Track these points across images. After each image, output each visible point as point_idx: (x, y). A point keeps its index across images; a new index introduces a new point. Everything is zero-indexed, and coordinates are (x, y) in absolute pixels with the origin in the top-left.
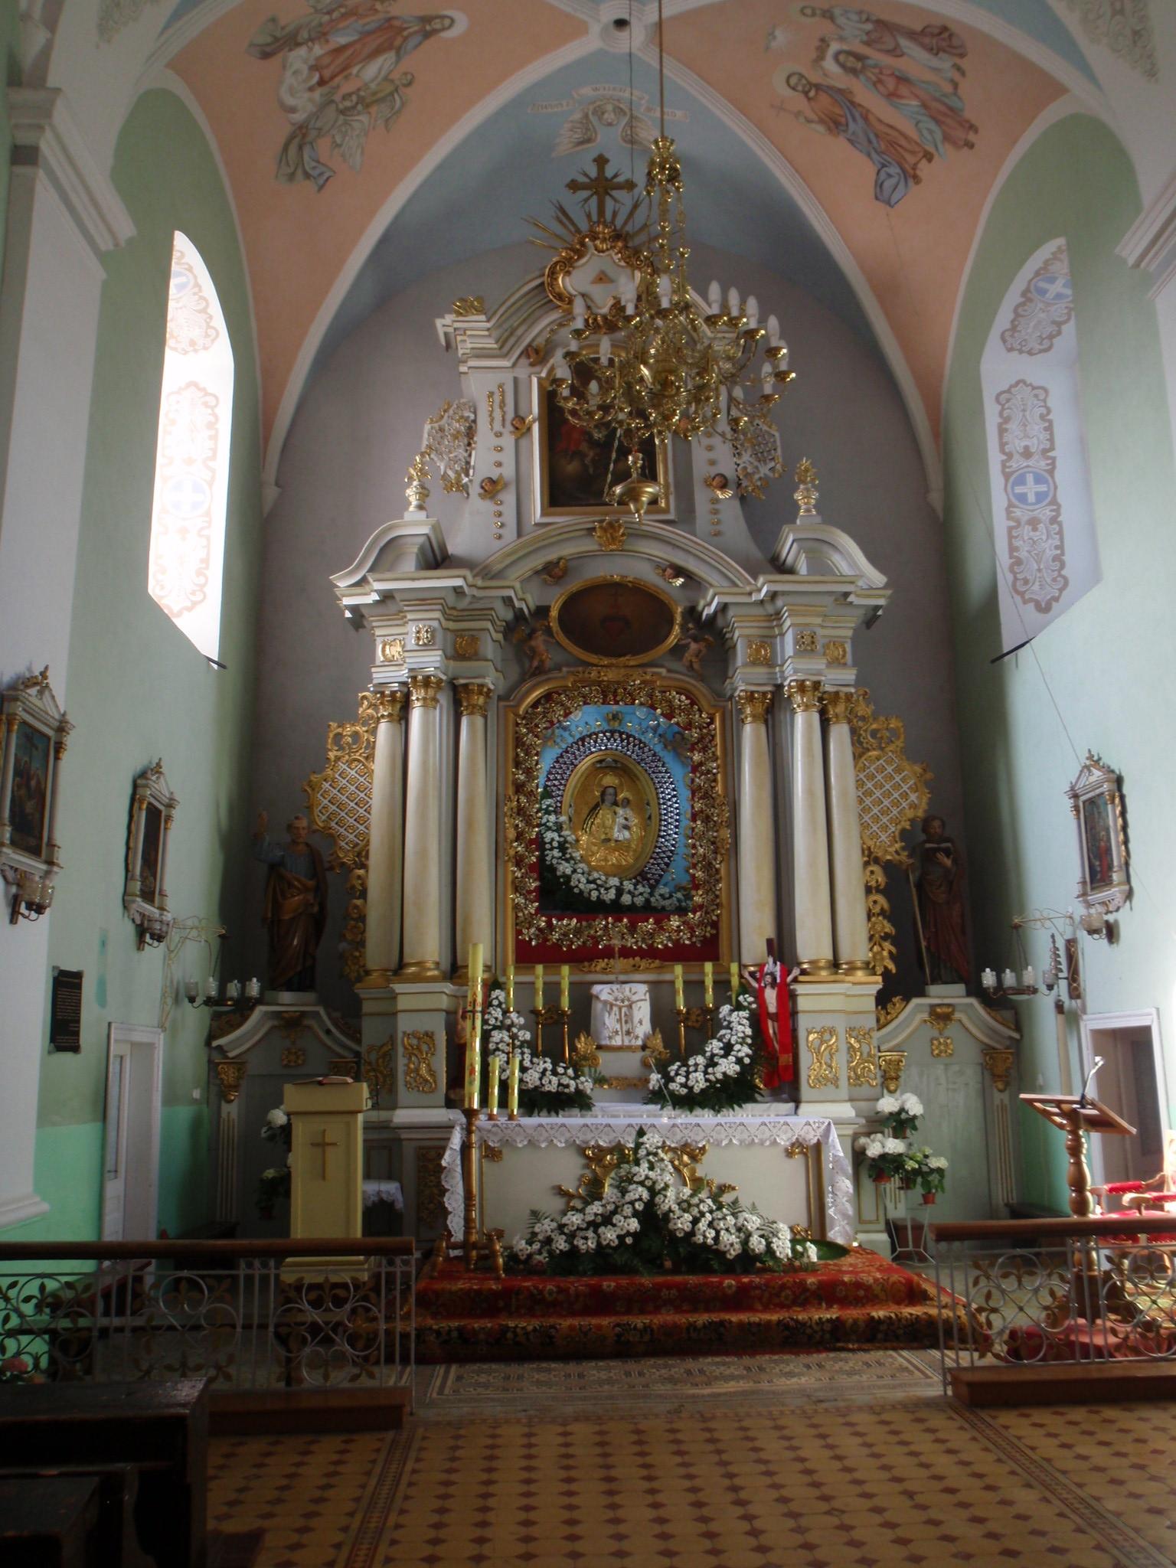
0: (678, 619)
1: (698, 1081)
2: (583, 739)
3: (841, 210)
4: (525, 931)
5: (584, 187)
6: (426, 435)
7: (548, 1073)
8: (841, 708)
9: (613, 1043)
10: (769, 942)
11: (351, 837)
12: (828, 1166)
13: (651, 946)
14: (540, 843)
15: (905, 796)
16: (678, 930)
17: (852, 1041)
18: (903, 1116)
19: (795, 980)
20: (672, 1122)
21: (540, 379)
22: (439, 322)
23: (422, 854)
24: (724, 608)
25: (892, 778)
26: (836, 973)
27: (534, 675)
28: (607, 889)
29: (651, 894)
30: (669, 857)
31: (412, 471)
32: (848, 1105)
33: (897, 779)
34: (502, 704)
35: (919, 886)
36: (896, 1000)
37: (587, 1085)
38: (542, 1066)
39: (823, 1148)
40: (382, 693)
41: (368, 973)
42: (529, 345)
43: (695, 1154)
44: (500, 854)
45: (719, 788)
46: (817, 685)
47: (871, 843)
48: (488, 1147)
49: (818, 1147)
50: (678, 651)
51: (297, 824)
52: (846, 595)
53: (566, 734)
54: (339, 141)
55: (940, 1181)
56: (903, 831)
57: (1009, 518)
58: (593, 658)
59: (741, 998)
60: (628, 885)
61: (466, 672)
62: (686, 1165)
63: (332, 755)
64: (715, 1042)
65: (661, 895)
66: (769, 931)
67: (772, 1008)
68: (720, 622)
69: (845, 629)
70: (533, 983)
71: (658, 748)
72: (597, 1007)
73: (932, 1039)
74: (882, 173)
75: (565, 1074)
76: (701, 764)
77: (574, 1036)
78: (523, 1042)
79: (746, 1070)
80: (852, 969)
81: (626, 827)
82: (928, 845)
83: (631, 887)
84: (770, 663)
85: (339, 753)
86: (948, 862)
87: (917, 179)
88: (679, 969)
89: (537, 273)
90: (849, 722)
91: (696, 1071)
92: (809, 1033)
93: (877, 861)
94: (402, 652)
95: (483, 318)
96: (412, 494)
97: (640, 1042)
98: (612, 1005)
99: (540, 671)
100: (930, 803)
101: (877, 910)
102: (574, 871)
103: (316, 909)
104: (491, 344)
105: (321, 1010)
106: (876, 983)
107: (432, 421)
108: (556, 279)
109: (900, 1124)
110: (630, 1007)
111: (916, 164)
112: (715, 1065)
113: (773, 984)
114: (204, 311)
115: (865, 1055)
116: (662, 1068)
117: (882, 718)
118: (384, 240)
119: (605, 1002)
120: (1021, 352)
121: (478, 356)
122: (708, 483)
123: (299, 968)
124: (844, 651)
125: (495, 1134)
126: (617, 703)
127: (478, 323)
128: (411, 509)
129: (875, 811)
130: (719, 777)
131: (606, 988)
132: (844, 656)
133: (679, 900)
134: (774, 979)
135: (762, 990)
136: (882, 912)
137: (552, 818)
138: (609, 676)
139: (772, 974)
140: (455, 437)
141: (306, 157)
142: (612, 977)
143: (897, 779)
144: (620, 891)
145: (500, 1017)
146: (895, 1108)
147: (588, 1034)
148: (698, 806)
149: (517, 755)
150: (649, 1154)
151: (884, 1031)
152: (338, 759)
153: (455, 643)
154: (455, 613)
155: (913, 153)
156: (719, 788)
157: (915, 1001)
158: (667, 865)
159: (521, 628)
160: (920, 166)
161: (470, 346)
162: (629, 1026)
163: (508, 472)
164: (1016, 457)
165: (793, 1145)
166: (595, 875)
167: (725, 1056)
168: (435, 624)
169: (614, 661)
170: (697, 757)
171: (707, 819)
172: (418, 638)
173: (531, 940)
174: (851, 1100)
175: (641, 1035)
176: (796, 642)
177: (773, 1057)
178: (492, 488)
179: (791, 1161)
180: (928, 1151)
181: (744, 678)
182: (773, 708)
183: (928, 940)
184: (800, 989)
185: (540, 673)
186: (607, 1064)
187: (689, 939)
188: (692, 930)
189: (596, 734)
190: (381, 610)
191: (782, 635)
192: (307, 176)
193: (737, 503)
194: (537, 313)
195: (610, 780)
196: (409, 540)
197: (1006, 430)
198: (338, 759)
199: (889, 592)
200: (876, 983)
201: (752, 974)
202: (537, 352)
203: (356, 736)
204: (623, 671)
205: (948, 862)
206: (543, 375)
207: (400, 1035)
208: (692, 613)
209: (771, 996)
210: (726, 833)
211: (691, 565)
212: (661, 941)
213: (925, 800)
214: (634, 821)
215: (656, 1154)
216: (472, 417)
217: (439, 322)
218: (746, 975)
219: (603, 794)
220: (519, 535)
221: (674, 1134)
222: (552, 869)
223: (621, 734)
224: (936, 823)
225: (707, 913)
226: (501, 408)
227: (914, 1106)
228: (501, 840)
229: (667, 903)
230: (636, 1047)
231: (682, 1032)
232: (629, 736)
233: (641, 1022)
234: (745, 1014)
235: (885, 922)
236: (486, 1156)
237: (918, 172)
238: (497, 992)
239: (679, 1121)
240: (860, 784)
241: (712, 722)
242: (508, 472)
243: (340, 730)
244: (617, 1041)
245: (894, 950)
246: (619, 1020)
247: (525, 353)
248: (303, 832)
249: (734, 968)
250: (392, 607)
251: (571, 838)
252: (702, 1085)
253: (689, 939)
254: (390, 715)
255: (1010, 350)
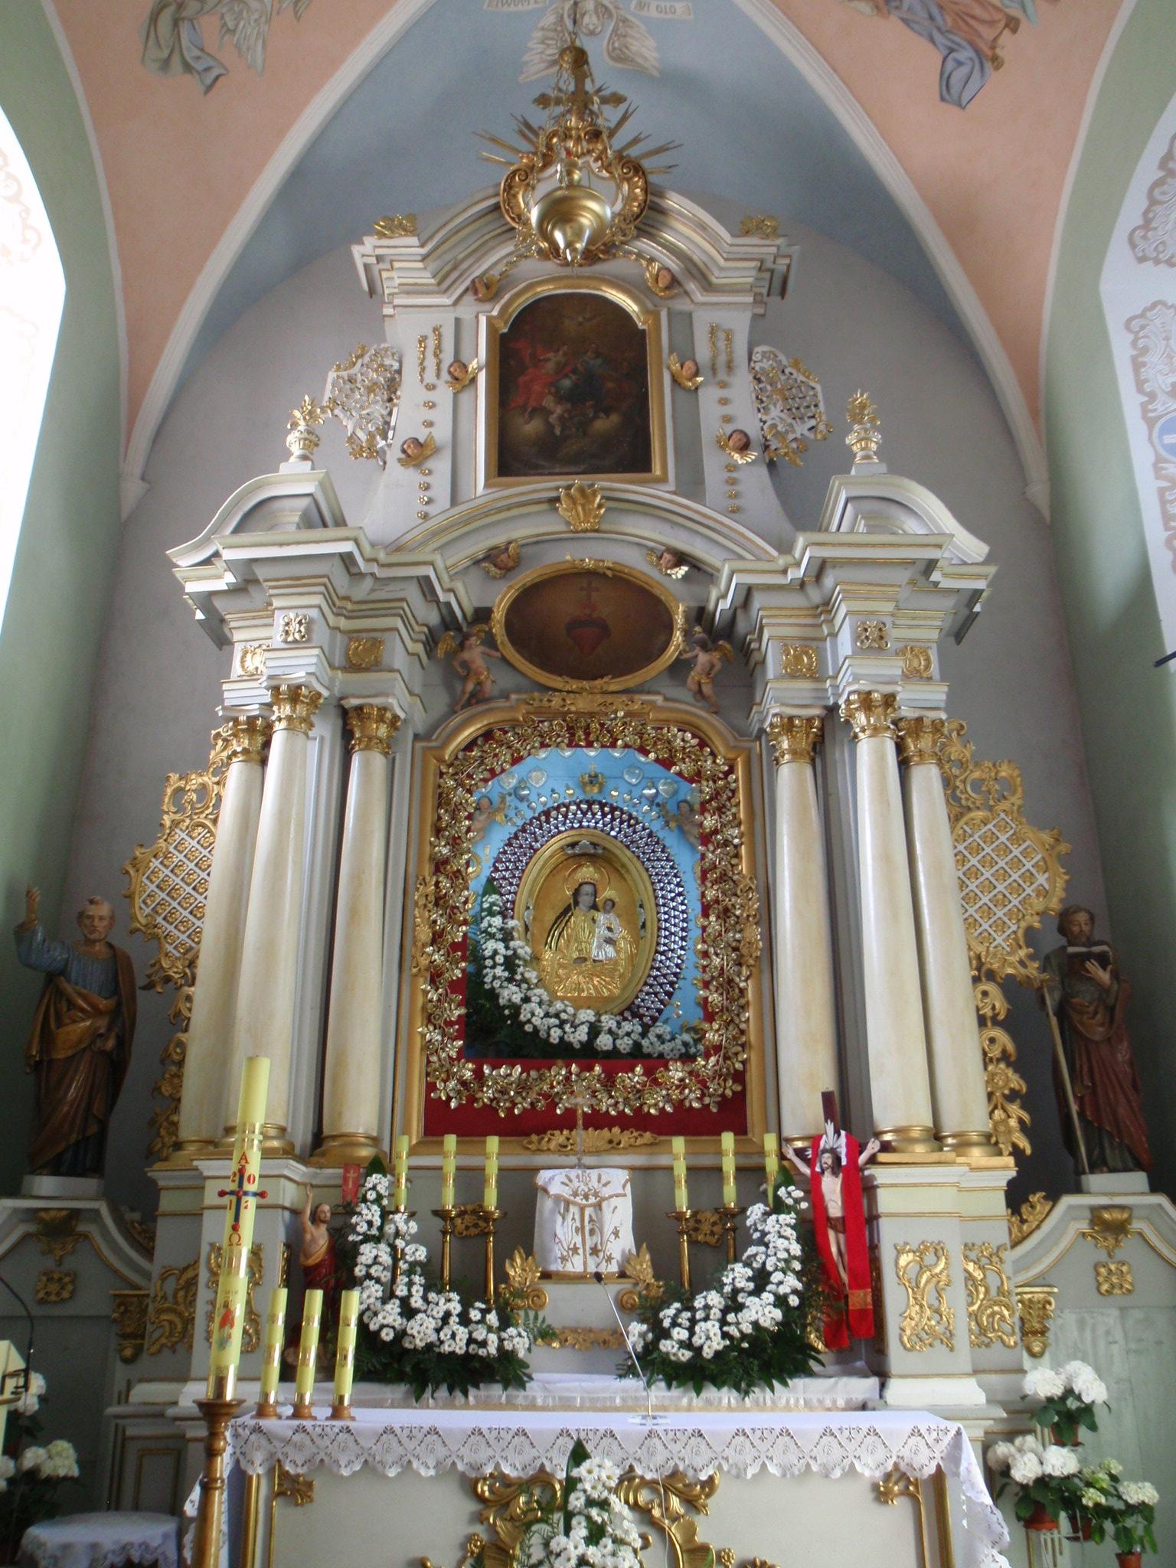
0: (679, 620)
1: (711, 1339)
2: (547, 813)
3: (899, 129)
4: (440, 1085)
5: (558, 102)
6: (329, 386)
7: (454, 1319)
8: (926, 742)
9: (569, 1268)
10: (827, 1097)
11: (183, 937)
12: (959, 1524)
13: (638, 1111)
14: (469, 950)
15: (1029, 877)
16: (682, 1085)
17: (971, 1267)
18: (1072, 1404)
19: (872, 1160)
20: (649, 1425)
21: (489, 320)
22: (357, 250)
23: (268, 950)
24: (747, 594)
25: (1007, 851)
26: (941, 1150)
27: (468, 704)
28: (575, 1026)
29: (644, 1035)
30: (672, 984)
31: (297, 414)
32: (972, 1382)
33: (1016, 852)
34: (419, 745)
35: (1062, 1012)
36: (1035, 1198)
37: (518, 1341)
38: (443, 1307)
39: (950, 1483)
40: (236, 720)
41: (178, 1146)
42: (480, 277)
43: (695, 1495)
44: (407, 964)
45: (744, 867)
46: (889, 700)
47: (981, 949)
48: (284, 1475)
49: (938, 1480)
50: (680, 668)
51: (92, 910)
52: (931, 565)
53: (523, 806)
54: (231, 25)
55: (1147, 1529)
56: (1030, 932)
57: (1158, 477)
58: (556, 681)
59: (782, 1192)
60: (608, 1021)
61: (359, 689)
62: (675, 1518)
63: (167, 820)
64: (738, 1267)
65: (659, 1037)
66: (827, 1081)
67: (835, 1207)
68: (741, 626)
69: (928, 627)
70: (440, 1168)
71: (656, 826)
72: (545, 1206)
73: (1096, 1267)
74: (950, 65)
75: (482, 1321)
76: (716, 832)
77: (504, 1255)
78: (413, 1265)
79: (792, 1319)
80: (963, 1144)
81: (610, 941)
82: (1071, 950)
83: (613, 1024)
84: (816, 675)
85: (177, 817)
86: (1104, 976)
87: (997, 61)
88: (679, 1143)
89: (491, 191)
90: (940, 764)
91: (706, 1319)
92: (899, 1252)
93: (991, 975)
94: (271, 656)
95: (414, 241)
96: (294, 442)
97: (614, 1268)
98: (568, 1203)
99: (476, 698)
100: (1069, 886)
101: (995, 1052)
102: (526, 1000)
103: (111, 1044)
104: (427, 279)
105: (103, 1208)
106: (1005, 1169)
107: (339, 368)
108: (515, 196)
109: (1066, 1418)
110: (598, 1206)
111: (995, 39)
112: (739, 1308)
113: (836, 1167)
114: (15, 198)
115: (993, 1292)
116: (649, 1312)
117: (988, 764)
118: (298, 175)
119: (558, 1198)
120: (1157, 262)
121: (408, 293)
122: (722, 444)
123: (74, 1137)
124: (928, 660)
125: (300, 1447)
126: (590, 745)
127: (408, 245)
128: (292, 459)
129: (985, 899)
130: (743, 850)
131: (559, 1175)
132: (927, 667)
133: (685, 1044)
134: (838, 1159)
135: (816, 1178)
136: (1005, 1057)
137: (497, 921)
138: (581, 704)
139: (833, 1151)
140: (370, 390)
141: (185, 42)
142: (573, 1160)
143: (1016, 852)
144: (594, 1030)
145: (377, 1221)
146: (1057, 1391)
147: (529, 1252)
148: (711, 894)
149: (440, 818)
150: (590, 1502)
151: (1021, 1249)
152: (175, 824)
153: (348, 649)
154: (350, 606)
155: (991, 23)
156: (744, 867)
157: (1067, 1201)
158: (669, 994)
159: (450, 637)
160: (1001, 41)
161: (398, 281)
162: (597, 1238)
163: (442, 433)
164: (1161, 397)
165: (887, 1477)
166: (559, 1006)
167: (757, 1292)
168: (314, 613)
169: (586, 684)
170: (710, 822)
171: (726, 913)
172: (287, 633)
173: (449, 1099)
174: (976, 1372)
175: (617, 1256)
176: (856, 637)
177: (839, 1295)
178: (417, 453)
179: (883, 1511)
180: (1116, 1468)
181: (780, 698)
182: (824, 740)
183: (1080, 1101)
184: (881, 1175)
185: (478, 702)
186: (561, 1305)
187: (700, 1099)
188: (703, 1084)
189: (567, 806)
190: (241, 602)
191: (834, 635)
192: (188, 68)
193: (763, 471)
194: (491, 244)
195: (587, 872)
196: (287, 503)
197: (1144, 364)
198: (175, 824)
199: (992, 570)
200: (1006, 1168)
201: (799, 1153)
202: (488, 287)
203: (203, 789)
204: (599, 699)
205: (1104, 976)
206: (495, 313)
207: (205, 1249)
208: (700, 615)
209: (832, 1188)
210: (755, 933)
211: (697, 548)
212: (655, 1103)
213: (1060, 884)
214: (621, 933)
215: (604, 1505)
216: (396, 366)
217: (357, 250)
218: (791, 1155)
219: (576, 893)
220: (454, 502)
221: (651, 1454)
222: (493, 995)
223: (602, 806)
224: (1082, 917)
225: (726, 1058)
226: (436, 355)
227: (1092, 1388)
228: (408, 943)
229: (666, 1048)
230: (610, 1275)
231: (686, 1250)
232: (613, 809)
233: (616, 1233)
234: (789, 1218)
235: (1010, 1072)
236: (281, 1494)
237: (998, 51)
238: (375, 1178)
239: (671, 1421)
240: (961, 859)
241: (731, 770)
242: (442, 433)
243: (182, 783)
244: (576, 1265)
245: (1026, 1117)
246: (580, 1230)
247: (473, 288)
248: (101, 926)
249: (770, 1142)
250: (257, 597)
251: (525, 951)
252: (717, 1344)
253: (700, 1099)
254: (245, 751)
255: (1142, 259)
